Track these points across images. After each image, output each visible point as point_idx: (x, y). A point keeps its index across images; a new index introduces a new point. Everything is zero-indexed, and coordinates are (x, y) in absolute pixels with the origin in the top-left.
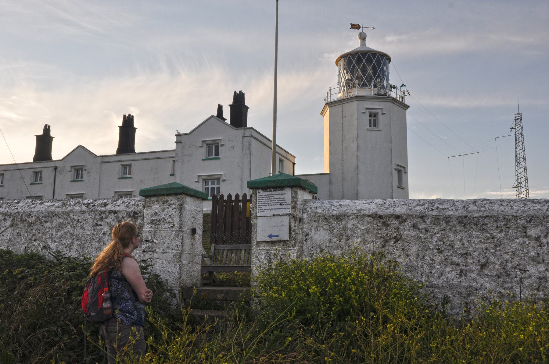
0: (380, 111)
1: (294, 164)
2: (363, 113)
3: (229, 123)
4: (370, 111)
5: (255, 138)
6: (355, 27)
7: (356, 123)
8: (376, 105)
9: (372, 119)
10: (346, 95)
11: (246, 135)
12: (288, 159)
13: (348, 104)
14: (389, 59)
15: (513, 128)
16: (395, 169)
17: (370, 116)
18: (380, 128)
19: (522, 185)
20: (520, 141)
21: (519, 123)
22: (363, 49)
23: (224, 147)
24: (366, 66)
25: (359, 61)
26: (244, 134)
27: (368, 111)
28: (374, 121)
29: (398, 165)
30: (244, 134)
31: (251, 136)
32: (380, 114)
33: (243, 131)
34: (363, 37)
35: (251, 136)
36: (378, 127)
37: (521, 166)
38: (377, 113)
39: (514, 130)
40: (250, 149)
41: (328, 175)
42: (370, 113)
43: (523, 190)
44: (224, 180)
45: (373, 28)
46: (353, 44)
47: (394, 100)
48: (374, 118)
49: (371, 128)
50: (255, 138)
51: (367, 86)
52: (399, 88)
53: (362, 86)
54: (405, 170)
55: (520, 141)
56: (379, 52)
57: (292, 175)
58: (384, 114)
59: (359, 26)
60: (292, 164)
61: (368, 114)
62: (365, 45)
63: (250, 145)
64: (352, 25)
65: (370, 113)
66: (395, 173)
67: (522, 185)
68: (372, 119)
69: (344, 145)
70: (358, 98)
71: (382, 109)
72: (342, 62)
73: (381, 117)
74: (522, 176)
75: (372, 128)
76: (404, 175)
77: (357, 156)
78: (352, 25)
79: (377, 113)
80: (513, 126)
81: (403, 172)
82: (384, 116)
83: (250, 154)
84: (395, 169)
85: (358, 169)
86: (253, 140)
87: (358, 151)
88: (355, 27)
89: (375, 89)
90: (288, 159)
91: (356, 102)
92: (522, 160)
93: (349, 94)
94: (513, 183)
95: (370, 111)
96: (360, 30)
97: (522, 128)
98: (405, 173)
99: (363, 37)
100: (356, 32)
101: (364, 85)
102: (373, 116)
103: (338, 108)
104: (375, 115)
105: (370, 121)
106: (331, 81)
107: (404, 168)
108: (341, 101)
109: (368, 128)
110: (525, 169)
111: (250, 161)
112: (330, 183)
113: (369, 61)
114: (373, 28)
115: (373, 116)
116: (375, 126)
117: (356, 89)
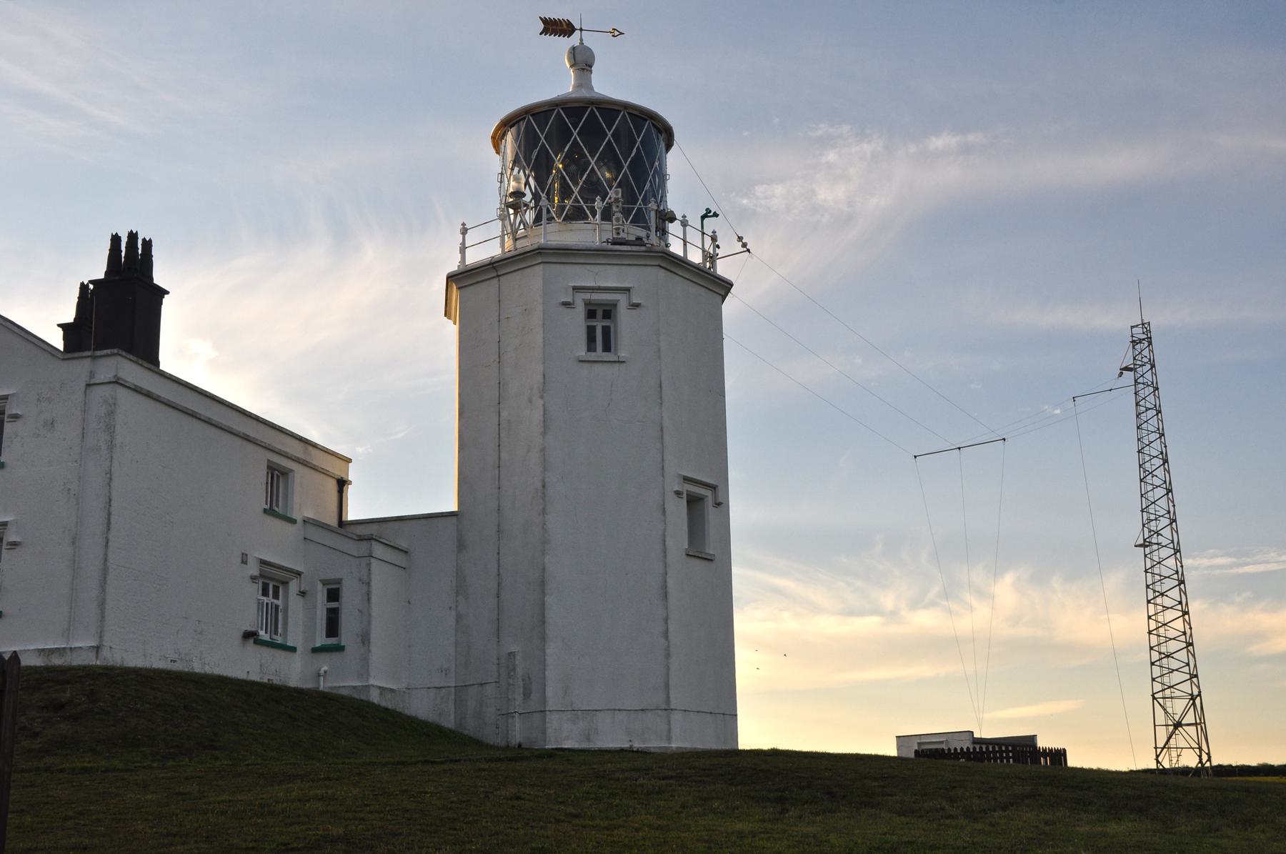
0: (622, 299)
1: (342, 484)
2: (566, 304)
3: (61, 347)
4: (587, 296)
5: (138, 390)
6: (556, 27)
7: (539, 338)
8: (609, 276)
9: (599, 325)
10: (509, 243)
11: (101, 377)
12: (314, 468)
13: (517, 276)
14: (666, 134)
15: (1127, 369)
16: (678, 493)
17: (591, 314)
18: (623, 354)
19: (1161, 539)
20: (1148, 411)
21: (1146, 352)
22: (584, 94)
23: (19, 423)
24: (590, 155)
25: (563, 134)
26: (92, 374)
27: (580, 298)
28: (606, 331)
29: (687, 480)
30: (92, 374)
31: (117, 382)
32: (622, 309)
33: (87, 362)
34: (582, 62)
35: (117, 382)
36: (616, 353)
37: (1157, 482)
38: (614, 305)
39: (1129, 375)
40: (110, 429)
41: (455, 519)
42: (588, 303)
43: (1165, 552)
44: (14, 545)
45: (616, 33)
46: (553, 81)
47: (680, 264)
48: (606, 323)
49: (592, 356)
50: (138, 390)
51: (585, 217)
52: (694, 220)
53: (568, 218)
54: (715, 496)
55: (1148, 411)
56: (626, 106)
57: (333, 522)
58: (637, 306)
59: (569, 24)
60: (332, 486)
61: (580, 310)
62: (592, 88)
63: (111, 414)
64: (545, 21)
65: (588, 303)
66: (678, 511)
67: (1161, 539)
68: (599, 325)
69: (504, 414)
70: (541, 253)
71: (628, 290)
72: (509, 141)
73: (626, 321)
74: (1162, 512)
75: (599, 354)
76: (711, 512)
77: (543, 450)
78: (545, 21)
79: (614, 305)
80: (1129, 362)
81: (709, 501)
82: (635, 312)
83: (111, 447)
84: (678, 493)
85: (544, 496)
86: (122, 393)
87: (544, 434)
88: (556, 27)
89: (607, 226)
90: (314, 468)
91: (539, 269)
92: (1158, 462)
93: (520, 244)
94: (1135, 532)
95: (587, 296)
96: (574, 40)
97: (1153, 366)
98: (718, 504)
99: (582, 62)
100: (565, 43)
101: (577, 215)
102: (600, 313)
103: (485, 291)
104: (609, 312)
105: (591, 331)
106: (473, 201)
107: (713, 488)
108: (492, 267)
109: (582, 352)
110: (1169, 491)
111: (110, 473)
112: (461, 546)
113: (592, 133)
114: (616, 33)
115: (600, 313)
116: (607, 348)
117: (552, 227)
